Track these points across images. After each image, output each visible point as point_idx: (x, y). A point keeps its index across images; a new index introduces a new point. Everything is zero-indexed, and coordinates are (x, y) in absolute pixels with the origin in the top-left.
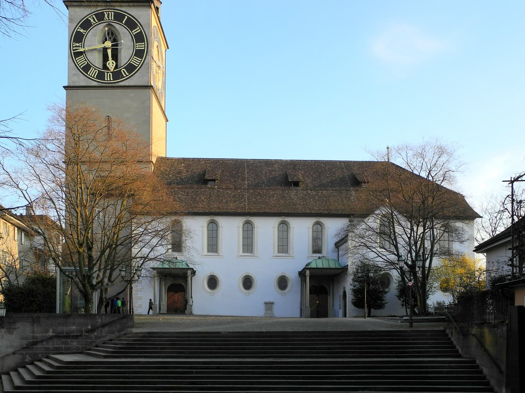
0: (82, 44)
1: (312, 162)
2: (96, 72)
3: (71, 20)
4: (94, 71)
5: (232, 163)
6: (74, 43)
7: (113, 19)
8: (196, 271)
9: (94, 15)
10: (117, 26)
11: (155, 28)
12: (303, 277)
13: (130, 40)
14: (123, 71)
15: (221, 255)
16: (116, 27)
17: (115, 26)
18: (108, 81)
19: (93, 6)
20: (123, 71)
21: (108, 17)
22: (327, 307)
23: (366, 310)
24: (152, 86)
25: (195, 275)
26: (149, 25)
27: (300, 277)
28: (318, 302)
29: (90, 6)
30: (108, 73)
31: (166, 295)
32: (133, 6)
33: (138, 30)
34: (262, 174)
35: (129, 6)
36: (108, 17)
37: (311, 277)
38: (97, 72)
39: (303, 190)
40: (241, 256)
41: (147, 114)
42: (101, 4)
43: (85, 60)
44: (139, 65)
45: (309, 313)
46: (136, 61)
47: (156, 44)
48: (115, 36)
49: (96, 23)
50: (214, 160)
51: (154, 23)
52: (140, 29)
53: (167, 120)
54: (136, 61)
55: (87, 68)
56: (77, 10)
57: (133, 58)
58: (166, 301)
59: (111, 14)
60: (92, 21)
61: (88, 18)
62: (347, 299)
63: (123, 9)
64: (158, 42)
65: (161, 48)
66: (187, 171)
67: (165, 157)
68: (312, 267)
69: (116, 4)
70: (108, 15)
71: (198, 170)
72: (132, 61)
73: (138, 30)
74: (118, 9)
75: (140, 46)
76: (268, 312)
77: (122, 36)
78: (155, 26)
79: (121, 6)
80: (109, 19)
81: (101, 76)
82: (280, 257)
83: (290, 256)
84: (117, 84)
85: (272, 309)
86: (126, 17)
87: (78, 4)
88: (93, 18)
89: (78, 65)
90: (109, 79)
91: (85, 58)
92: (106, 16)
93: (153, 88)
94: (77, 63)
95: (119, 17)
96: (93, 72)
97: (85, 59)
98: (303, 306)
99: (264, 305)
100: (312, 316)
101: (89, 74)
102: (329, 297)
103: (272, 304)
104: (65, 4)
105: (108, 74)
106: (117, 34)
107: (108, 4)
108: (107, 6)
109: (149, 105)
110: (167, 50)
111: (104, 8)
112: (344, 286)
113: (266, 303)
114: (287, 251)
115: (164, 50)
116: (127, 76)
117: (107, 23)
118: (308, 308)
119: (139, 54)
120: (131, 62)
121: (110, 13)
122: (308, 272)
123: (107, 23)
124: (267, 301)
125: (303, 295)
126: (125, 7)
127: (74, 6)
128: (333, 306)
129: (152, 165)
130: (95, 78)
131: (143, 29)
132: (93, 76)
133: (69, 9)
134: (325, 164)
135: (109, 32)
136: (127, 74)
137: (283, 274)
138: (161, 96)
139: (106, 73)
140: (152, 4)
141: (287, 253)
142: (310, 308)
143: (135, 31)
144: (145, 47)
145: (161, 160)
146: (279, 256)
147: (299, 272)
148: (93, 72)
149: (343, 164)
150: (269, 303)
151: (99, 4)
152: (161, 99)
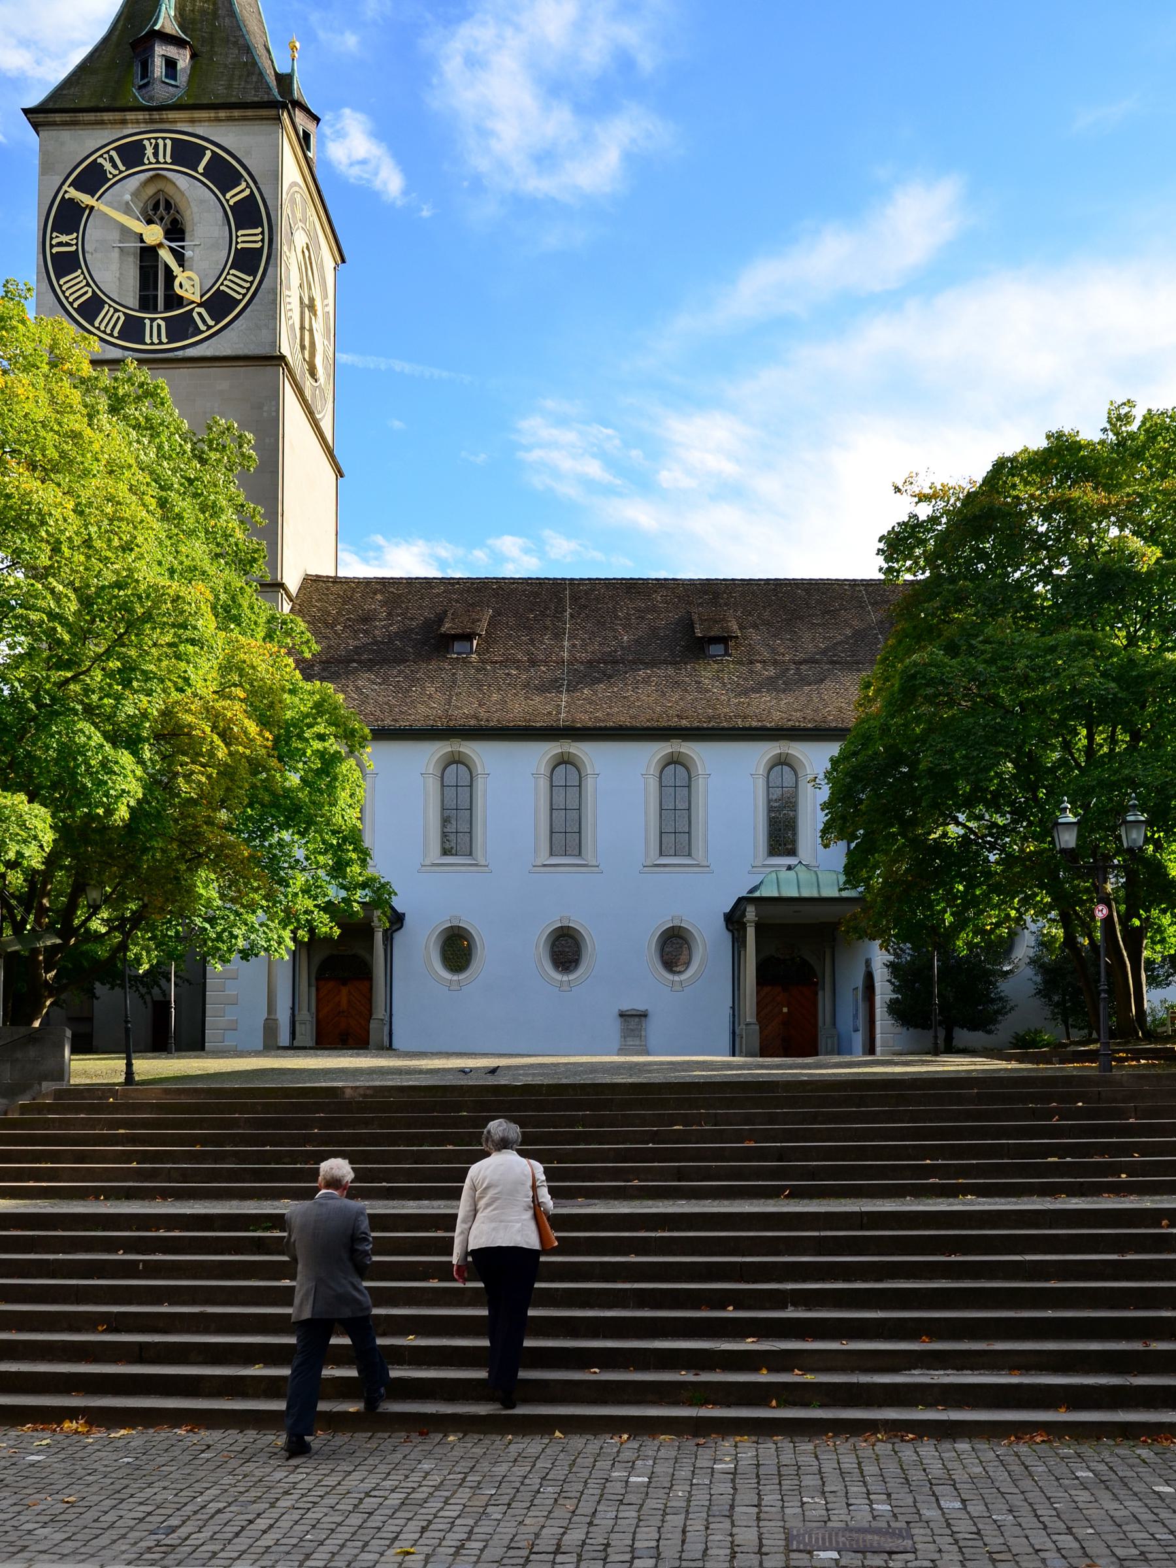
0: (77, 238)
1: (769, 584)
2: (119, 318)
3: (46, 167)
4: (112, 316)
5: (526, 590)
6: (54, 234)
7: (169, 160)
8: (404, 914)
9: (112, 149)
10: (182, 182)
11: (297, 189)
12: (737, 930)
13: (220, 223)
14: (200, 314)
15: (483, 863)
16: (178, 183)
17: (174, 180)
18: (152, 344)
19: (113, 123)
20: (200, 314)
21: (156, 154)
22: (815, 1025)
23: (942, 1034)
24: (282, 358)
25: (401, 927)
26: (276, 175)
27: (728, 929)
28: (785, 1010)
29: (102, 122)
30: (152, 320)
31: (313, 989)
32: (230, 119)
33: (242, 191)
34: (617, 617)
35: (218, 120)
36: (156, 154)
37: (759, 927)
38: (122, 318)
39: (741, 663)
40: (545, 865)
41: (267, 440)
42: (133, 117)
43: (88, 284)
44: (244, 295)
45: (756, 1044)
46: (236, 284)
47: (300, 239)
48: (178, 212)
49: (121, 172)
50: (473, 584)
51: (291, 172)
52: (248, 186)
53: (339, 473)
54: (236, 284)
55: (91, 309)
56: (66, 135)
57: (228, 273)
58: (313, 1010)
59: (165, 145)
60: (108, 166)
61: (96, 159)
62: (878, 999)
63: (200, 131)
64: (309, 235)
65: (318, 254)
66: (390, 614)
67: (333, 574)
68: (764, 895)
69: (177, 116)
70: (156, 147)
71: (422, 613)
72: (225, 283)
73: (242, 191)
74: (182, 129)
75: (249, 238)
76: (631, 1043)
77: (195, 209)
78: (294, 184)
79: (192, 121)
80: (157, 159)
81: (132, 330)
82: (667, 869)
83: (697, 865)
84: (180, 354)
85: (643, 1033)
86: (208, 154)
87: (68, 119)
88: (112, 159)
89: (67, 298)
90: (156, 341)
91: (85, 278)
92: (149, 151)
93: (286, 365)
94: (63, 292)
95: (186, 154)
96: (110, 319)
97: (87, 282)
98: (739, 1025)
99: (619, 1020)
100: (763, 1053)
101: (61, 282)
102: (820, 993)
103: (643, 1019)
104: (28, 119)
105: (155, 324)
106: (182, 206)
107: (156, 116)
108: (152, 121)
109: (274, 414)
110: (342, 266)
111: (143, 128)
112: (868, 957)
113: (622, 1015)
114: (690, 849)
115: (329, 264)
116: (209, 327)
117: (151, 173)
118: (753, 1027)
119: (247, 261)
120: (222, 288)
121: (160, 142)
122: (751, 913)
123: (151, 173)
124: (626, 1006)
125: (739, 989)
126: (206, 124)
127: (54, 124)
128: (834, 1024)
129: (284, 596)
130: (116, 338)
131: (258, 189)
132: (108, 331)
133: (41, 133)
134: (807, 591)
135: (159, 201)
136: (211, 323)
137: (677, 923)
138: (318, 397)
139: (147, 322)
140: (285, 114)
141: (689, 855)
142: (758, 1027)
143: (236, 195)
144: (262, 240)
145: (312, 582)
146: (665, 865)
147: (725, 914)
148: (110, 319)
149: (862, 588)
150: (634, 1013)
151: (130, 116)
152: (319, 408)
